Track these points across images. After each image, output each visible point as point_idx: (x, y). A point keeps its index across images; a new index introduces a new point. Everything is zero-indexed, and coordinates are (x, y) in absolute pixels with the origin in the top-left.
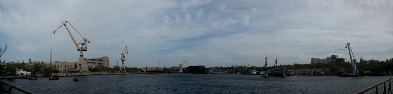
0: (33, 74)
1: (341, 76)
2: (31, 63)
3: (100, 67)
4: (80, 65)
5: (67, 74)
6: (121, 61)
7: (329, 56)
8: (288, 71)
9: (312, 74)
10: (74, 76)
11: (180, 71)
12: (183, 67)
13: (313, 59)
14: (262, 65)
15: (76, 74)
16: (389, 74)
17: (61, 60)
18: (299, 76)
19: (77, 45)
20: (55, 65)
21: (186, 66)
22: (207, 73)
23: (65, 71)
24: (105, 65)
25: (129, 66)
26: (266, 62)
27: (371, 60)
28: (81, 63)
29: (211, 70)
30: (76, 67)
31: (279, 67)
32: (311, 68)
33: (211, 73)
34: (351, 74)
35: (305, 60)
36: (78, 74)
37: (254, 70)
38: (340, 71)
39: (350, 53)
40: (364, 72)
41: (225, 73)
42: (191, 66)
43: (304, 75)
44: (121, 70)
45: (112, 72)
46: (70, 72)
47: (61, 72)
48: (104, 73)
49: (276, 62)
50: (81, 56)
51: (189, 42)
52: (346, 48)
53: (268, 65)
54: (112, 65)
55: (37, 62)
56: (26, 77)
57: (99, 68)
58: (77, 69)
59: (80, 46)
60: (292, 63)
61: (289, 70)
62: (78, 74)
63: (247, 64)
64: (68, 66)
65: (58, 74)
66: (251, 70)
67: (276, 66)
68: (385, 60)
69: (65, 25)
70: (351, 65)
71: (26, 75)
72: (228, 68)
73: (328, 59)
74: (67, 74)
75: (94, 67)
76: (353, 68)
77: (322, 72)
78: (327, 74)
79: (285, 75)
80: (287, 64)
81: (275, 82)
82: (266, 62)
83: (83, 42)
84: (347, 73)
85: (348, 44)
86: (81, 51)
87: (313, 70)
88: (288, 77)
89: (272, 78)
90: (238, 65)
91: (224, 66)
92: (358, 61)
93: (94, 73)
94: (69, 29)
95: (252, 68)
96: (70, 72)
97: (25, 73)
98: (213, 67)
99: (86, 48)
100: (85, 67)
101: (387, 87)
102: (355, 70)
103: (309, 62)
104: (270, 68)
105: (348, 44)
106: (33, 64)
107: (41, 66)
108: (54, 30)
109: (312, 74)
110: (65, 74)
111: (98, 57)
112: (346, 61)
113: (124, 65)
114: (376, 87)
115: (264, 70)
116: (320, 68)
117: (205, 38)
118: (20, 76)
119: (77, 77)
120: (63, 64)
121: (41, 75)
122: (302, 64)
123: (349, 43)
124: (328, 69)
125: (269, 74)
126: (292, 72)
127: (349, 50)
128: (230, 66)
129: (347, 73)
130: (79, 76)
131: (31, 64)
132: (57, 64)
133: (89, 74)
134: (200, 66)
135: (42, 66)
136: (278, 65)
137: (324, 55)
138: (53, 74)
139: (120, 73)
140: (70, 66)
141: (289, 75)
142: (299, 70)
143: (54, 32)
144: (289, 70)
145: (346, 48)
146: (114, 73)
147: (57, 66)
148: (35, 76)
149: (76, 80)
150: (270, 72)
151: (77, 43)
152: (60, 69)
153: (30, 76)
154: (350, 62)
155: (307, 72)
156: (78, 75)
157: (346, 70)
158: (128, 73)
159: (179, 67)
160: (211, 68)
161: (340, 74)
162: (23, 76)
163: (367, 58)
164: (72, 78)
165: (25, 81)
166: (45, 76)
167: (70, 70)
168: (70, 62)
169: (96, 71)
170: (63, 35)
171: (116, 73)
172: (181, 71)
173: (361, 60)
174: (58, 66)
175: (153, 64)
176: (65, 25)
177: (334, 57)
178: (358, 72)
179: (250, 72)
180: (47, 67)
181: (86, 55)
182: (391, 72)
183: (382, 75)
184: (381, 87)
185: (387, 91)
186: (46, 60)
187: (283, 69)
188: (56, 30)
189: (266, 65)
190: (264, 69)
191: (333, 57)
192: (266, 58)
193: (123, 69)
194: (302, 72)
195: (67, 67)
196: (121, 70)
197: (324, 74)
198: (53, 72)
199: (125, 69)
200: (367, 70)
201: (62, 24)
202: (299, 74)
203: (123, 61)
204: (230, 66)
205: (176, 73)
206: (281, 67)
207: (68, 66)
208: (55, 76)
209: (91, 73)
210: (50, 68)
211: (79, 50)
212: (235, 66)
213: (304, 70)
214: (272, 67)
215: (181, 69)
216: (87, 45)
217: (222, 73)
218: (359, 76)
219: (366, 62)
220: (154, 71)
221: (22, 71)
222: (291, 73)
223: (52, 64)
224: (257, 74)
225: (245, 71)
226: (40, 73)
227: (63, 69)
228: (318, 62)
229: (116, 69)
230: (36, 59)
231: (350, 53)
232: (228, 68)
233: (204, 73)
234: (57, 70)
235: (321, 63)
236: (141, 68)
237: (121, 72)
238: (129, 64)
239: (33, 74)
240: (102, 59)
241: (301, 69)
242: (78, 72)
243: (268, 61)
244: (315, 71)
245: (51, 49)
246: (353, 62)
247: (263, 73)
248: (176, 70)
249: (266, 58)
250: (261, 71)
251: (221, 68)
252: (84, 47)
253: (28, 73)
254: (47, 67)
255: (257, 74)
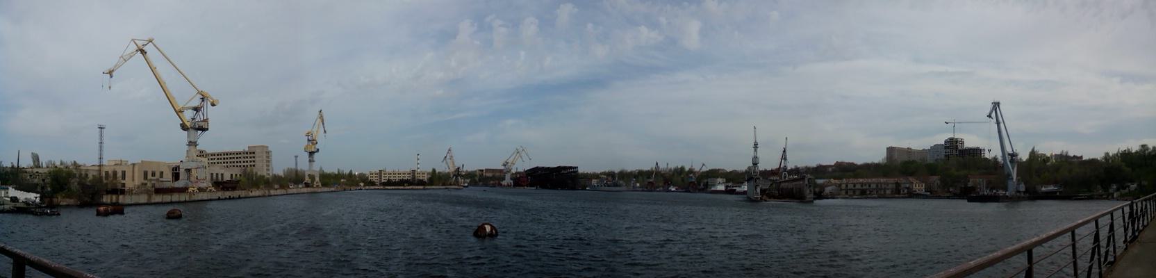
0: (47, 200)
1: (971, 200)
2: (38, 167)
3: (243, 179)
4: (188, 171)
5: (150, 196)
6: (307, 155)
7: (941, 139)
8: (816, 185)
9: (888, 192)
10: (171, 203)
11: (504, 183)
12: (514, 171)
13: (891, 150)
14: (742, 165)
15: (175, 197)
16: (1109, 197)
17: (132, 157)
18: (851, 197)
19: (179, 112)
20: (115, 173)
21: (522, 166)
22: (584, 188)
23: (142, 189)
24: (261, 170)
25: (331, 169)
26: (755, 158)
27: (1061, 156)
28: (191, 165)
29: (594, 182)
30: (176, 177)
31: (791, 172)
32: (885, 176)
33: (594, 189)
34: (1001, 192)
35: (868, 149)
36: (183, 197)
37: (720, 180)
38: (970, 184)
39: (999, 132)
40: (1038, 188)
41: (635, 189)
42: (537, 169)
43: (863, 194)
44: (307, 179)
45: (282, 187)
46: (159, 191)
47: (131, 192)
48: (256, 193)
49: (784, 158)
50: (192, 144)
51: (540, 97)
52: (990, 116)
53: (762, 167)
54: (279, 167)
55: (58, 164)
56: (25, 209)
57: (243, 179)
58: (180, 184)
59: (188, 115)
60: (829, 160)
61: (820, 181)
62: (183, 197)
63: (697, 161)
64: (153, 174)
65: (121, 199)
66: (710, 181)
67: (785, 169)
68: (1099, 155)
69: (143, 52)
70: (1003, 166)
71: (26, 202)
72: (641, 173)
73: (936, 148)
74: (150, 196)
75: (227, 177)
76: (1009, 176)
77: (918, 187)
78: (931, 194)
79: (809, 196)
80: (813, 164)
81: (781, 218)
82: (755, 158)
83: (196, 103)
84: (992, 189)
85: (996, 105)
86: (192, 132)
87: (892, 180)
88: (817, 202)
89: (773, 202)
90: (672, 166)
91: (631, 167)
92: (1024, 156)
93: (228, 194)
94: (155, 63)
95: (714, 174)
96: (159, 191)
97: (22, 196)
98: (598, 171)
99: (206, 121)
100: (203, 176)
101: (1104, 234)
102: (1015, 183)
103: (879, 157)
104: (766, 174)
105: (996, 105)
106: (46, 171)
107: (70, 175)
108: (111, 67)
109: (888, 192)
110: (143, 199)
111: (240, 149)
112: (988, 155)
113: (316, 167)
114: (1072, 230)
115: (748, 180)
116: (912, 174)
117: (595, 82)
118: (7, 207)
119: (176, 207)
120: (136, 169)
121: (71, 201)
122: (859, 162)
123: (998, 104)
124: (935, 180)
125: (763, 191)
126: (831, 186)
127: (998, 123)
128: (646, 168)
129: (992, 189)
130: (186, 202)
131: (40, 171)
132: (119, 170)
133: (215, 196)
134: (565, 168)
135: (74, 176)
136: (790, 166)
137: (923, 138)
138: (106, 199)
139: (305, 190)
140: (158, 175)
141: (819, 196)
142: (850, 179)
143: (110, 73)
144: (820, 181)
145: (990, 116)
146: (290, 191)
147: (120, 174)
148: (51, 206)
149: (172, 216)
150: (766, 185)
151: (180, 105)
152: (129, 184)
153: (38, 206)
154: (1000, 159)
155: (874, 186)
156: (182, 199)
157: (989, 183)
158: (326, 189)
159: (501, 171)
160: (596, 176)
161: (969, 194)
162: (18, 205)
163: (1050, 148)
164: (166, 210)
165: (22, 218)
166: (83, 205)
167: (157, 186)
168: (158, 164)
169: (234, 189)
170: (137, 85)
171: (295, 191)
172: (508, 180)
173: (1033, 154)
174: (124, 173)
175: (399, 163)
176: (143, 52)
177: (952, 144)
178: (1022, 188)
179: (706, 185)
180: (90, 177)
181: (207, 142)
182: (1118, 190)
183: (1090, 198)
184: (1085, 234)
185: (1103, 243)
186: (86, 157)
187: (803, 179)
188: (117, 66)
189: (755, 164)
190: (749, 176)
191: (952, 144)
192: (756, 145)
193: (312, 177)
194: (858, 186)
195: (149, 177)
196: (307, 179)
197: (923, 192)
198: (108, 192)
199: (317, 179)
200: (1048, 183)
201: (133, 48)
202: (849, 193)
203: (311, 153)
204: (647, 167)
205: (494, 186)
206: (796, 171)
207: (153, 174)
208: (112, 204)
209: (220, 194)
210: (98, 180)
211: (184, 127)
212: (662, 166)
213: (865, 181)
214: (773, 173)
215: (508, 176)
216: (210, 112)
217: (624, 188)
218: (1024, 199)
219: (1046, 160)
220: (402, 183)
221: (12, 192)
222: (828, 190)
223: (105, 169)
224: (729, 191)
225: (691, 183)
226: (69, 197)
227: (137, 182)
228: (905, 158)
229: (296, 178)
230: (55, 155)
231: (999, 132)
232: (641, 175)
233: (574, 189)
234: (119, 187)
235: (914, 162)
236: (367, 172)
237: (307, 185)
238: (328, 163)
239: (47, 200)
240: (251, 153)
241: (856, 177)
242: (184, 190)
243: (1011, 124)
244: (898, 184)
245: (102, 123)
246: (1008, 158)
247: (745, 188)
248: (493, 178)
249: (756, 145)
250: (740, 183)
251: (624, 176)
252: (200, 117)
253: (32, 196)
254: (90, 177)
255: (729, 191)
